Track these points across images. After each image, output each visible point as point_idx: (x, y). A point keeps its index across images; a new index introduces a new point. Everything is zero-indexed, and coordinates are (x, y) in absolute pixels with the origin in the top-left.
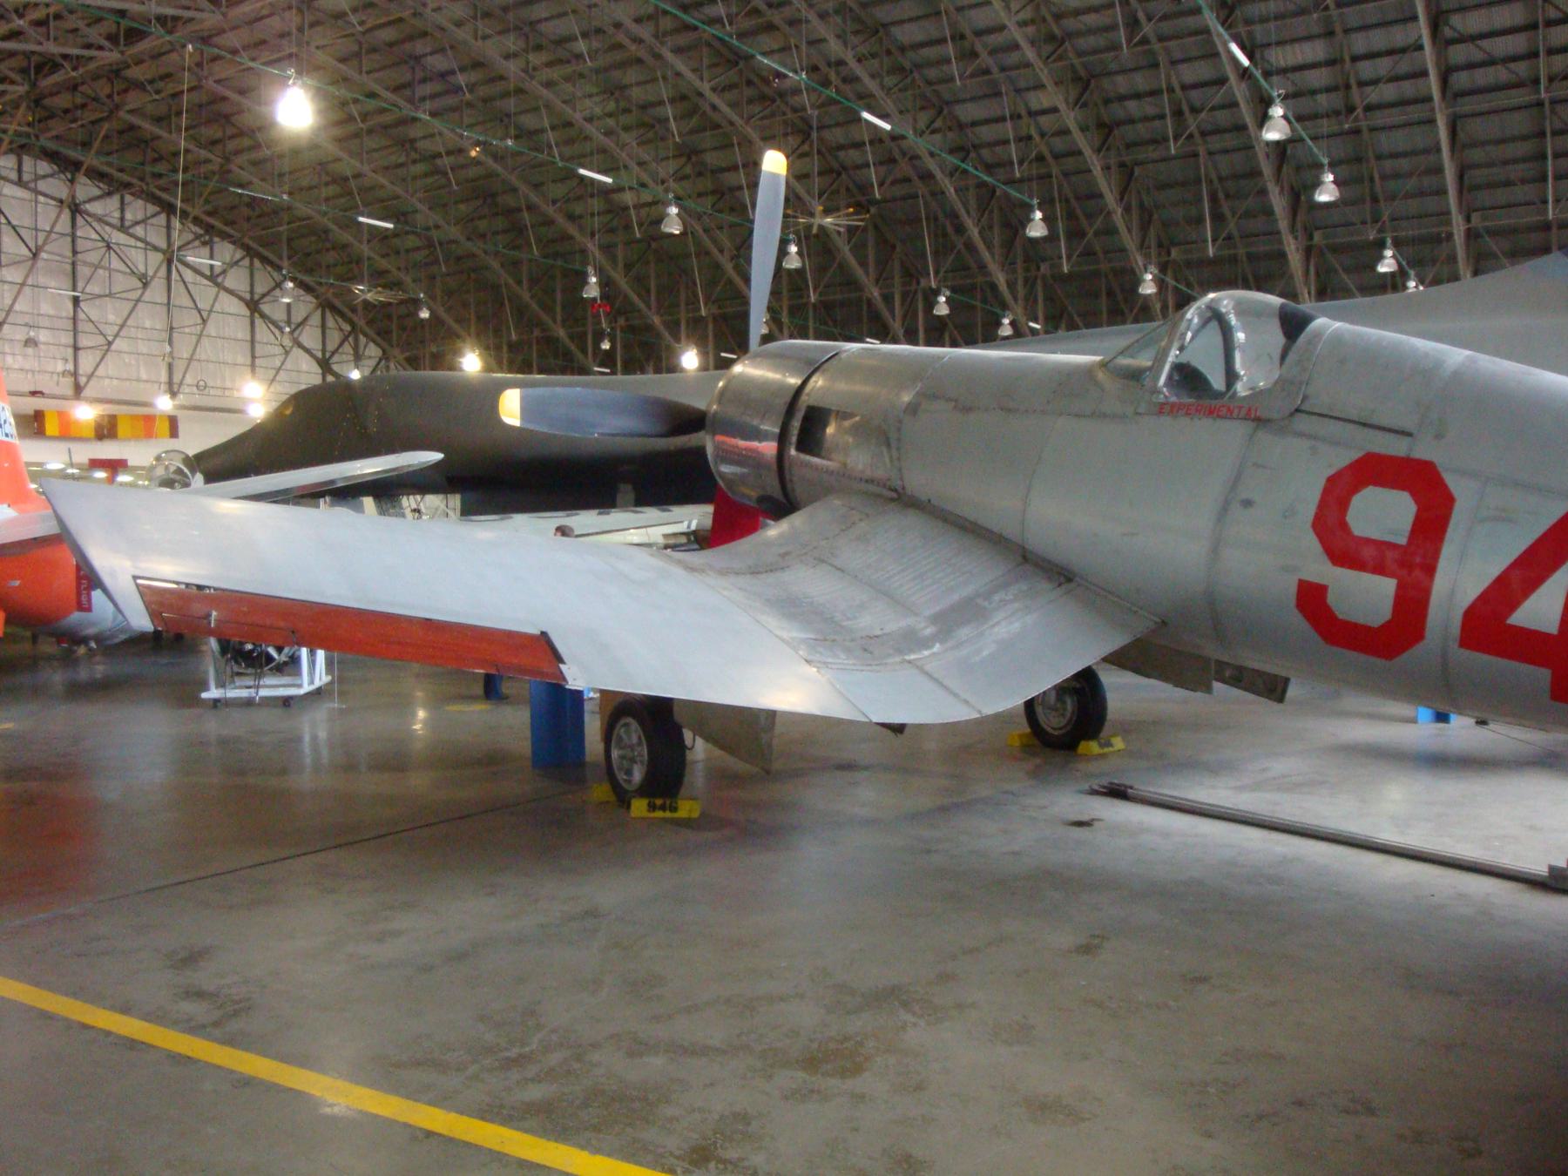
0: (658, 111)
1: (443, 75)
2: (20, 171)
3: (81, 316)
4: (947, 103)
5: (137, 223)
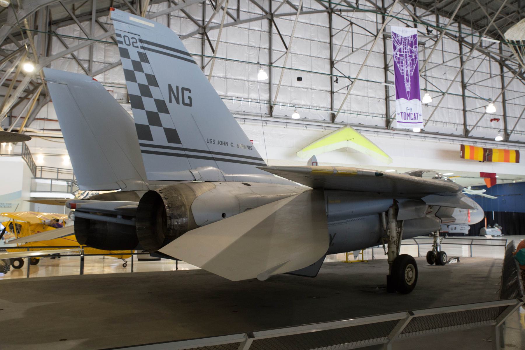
3: (467, 93)
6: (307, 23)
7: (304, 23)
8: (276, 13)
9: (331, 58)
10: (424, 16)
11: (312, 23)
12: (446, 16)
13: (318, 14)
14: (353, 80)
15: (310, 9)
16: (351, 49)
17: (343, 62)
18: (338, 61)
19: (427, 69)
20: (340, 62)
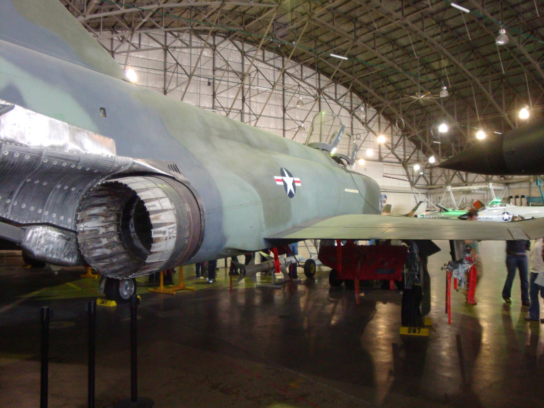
0: (461, 30)
1: (368, 24)
2: (263, 56)
3: (287, 117)
4: (535, 29)
5: (307, 78)
6: (145, 59)
7: (142, 58)
8: (117, 51)
9: (283, 106)
10: (251, 51)
11: (149, 58)
12: (271, 52)
13: (155, 51)
14: (258, 117)
15: (148, 46)
16: (257, 91)
17: (176, 90)
18: (171, 90)
19: (251, 96)
20: (173, 91)
